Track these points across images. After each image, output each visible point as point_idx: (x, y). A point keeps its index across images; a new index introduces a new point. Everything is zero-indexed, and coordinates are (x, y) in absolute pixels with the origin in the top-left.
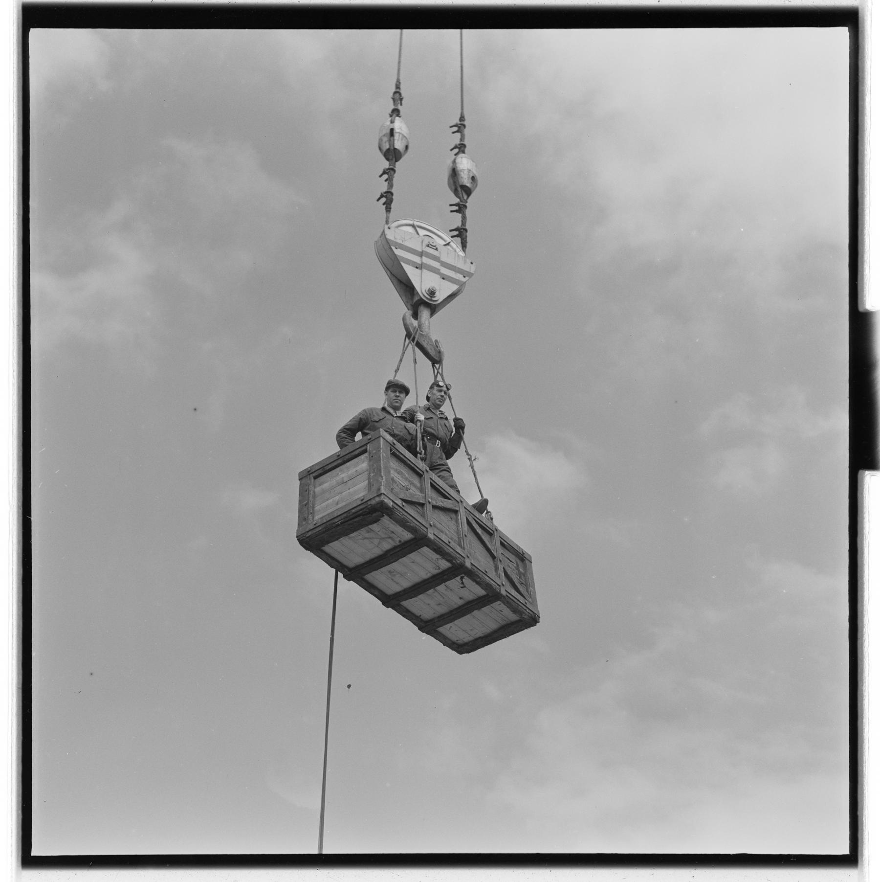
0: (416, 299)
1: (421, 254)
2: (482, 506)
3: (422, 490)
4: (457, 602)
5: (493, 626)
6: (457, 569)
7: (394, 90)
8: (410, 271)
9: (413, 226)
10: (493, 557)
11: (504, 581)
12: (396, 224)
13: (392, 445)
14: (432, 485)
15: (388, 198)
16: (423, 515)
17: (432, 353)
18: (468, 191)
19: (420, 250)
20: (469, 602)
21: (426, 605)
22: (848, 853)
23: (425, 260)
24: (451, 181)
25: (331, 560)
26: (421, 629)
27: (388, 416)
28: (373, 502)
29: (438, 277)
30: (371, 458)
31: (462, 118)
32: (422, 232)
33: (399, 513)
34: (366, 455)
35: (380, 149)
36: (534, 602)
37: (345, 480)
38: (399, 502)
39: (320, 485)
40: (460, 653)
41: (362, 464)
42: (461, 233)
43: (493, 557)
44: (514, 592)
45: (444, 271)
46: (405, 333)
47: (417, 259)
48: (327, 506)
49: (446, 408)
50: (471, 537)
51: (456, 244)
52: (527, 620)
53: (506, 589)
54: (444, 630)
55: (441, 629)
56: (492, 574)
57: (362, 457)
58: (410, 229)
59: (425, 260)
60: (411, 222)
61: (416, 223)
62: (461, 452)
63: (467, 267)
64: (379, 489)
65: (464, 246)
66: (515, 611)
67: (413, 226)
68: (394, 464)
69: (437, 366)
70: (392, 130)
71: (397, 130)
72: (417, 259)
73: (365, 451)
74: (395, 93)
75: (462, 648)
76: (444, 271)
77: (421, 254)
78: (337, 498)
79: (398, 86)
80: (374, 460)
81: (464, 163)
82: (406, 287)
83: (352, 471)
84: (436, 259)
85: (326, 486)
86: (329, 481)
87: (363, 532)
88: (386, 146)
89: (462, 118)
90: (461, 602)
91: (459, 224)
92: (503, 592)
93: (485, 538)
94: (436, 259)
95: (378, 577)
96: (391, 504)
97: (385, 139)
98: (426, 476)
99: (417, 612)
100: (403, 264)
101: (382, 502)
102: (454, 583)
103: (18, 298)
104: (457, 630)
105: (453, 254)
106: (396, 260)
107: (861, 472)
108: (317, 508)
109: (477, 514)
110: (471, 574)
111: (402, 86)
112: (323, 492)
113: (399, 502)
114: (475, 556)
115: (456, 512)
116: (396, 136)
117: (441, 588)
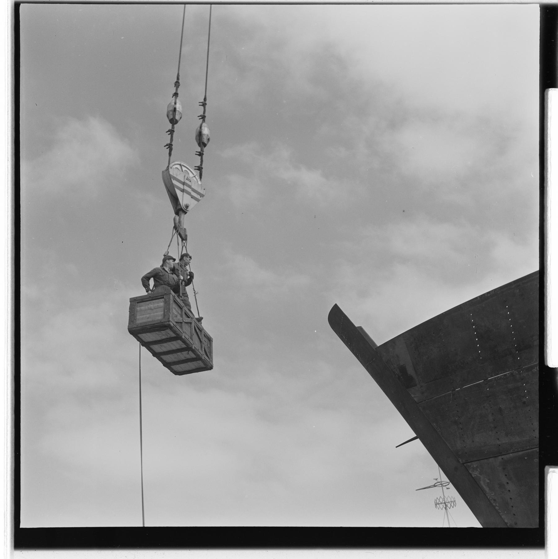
0: (179, 207)
1: (184, 184)
2: (200, 320)
3: (182, 316)
4: (183, 358)
5: (194, 367)
6: (188, 348)
7: (176, 80)
8: (178, 193)
9: (180, 165)
10: (201, 341)
11: (203, 353)
12: (173, 164)
13: (174, 297)
14: (185, 313)
15: (170, 146)
16: (181, 327)
17: (183, 236)
18: (205, 145)
19: (183, 181)
20: (188, 359)
21: (169, 358)
22: (538, 527)
23: (186, 188)
24: (198, 138)
25: (139, 339)
26: (164, 365)
27: (167, 274)
28: (166, 324)
29: (190, 197)
30: (165, 302)
31: (205, 99)
32: (184, 169)
33: (175, 328)
34: (163, 299)
35: (168, 116)
36: (212, 361)
37: (152, 308)
38: (175, 324)
39: (140, 307)
40: (176, 374)
41: (160, 303)
42: (200, 169)
43: (201, 341)
44: (206, 357)
45: (193, 194)
46: (173, 225)
47: (181, 186)
48: (143, 318)
49: (188, 267)
50: (195, 334)
51: (196, 173)
52: (209, 367)
53: (204, 357)
54: (152, 347)
55: (172, 367)
56: (200, 351)
57: (161, 300)
58: (178, 167)
59: (186, 188)
60: (179, 163)
61: (182, 164)
62: (191, 285)
63: (202, 192)
64: (169, 318)
65: (201, 177)
66: (205, 364)
67: (180, 165)
68: (174, 306)
69: (184, 241)
70: (175, 109)
71: (177, 109)
72: (181, 186)
73: (163, 298)
74: (176, 82)
75: (176, 373)
76: (193, 194)
77: (184, 184)
78: (148, 316)
79: (178, 79)
80: (167, 303)
81: (206, 131)
82: (175, 199)
83: (156, 305)
84: (190, 187)
85: (142, 308)
86: (143, 307)
87: (157, 332)
88: (171, 117)
89: (205, 99)
90: (184, 359)
91: (198, 164)
92: (203, 358)
93: (199, 333)
94: (190, 187)
95: (164, 357)
96: (172, 325)
97: (171, 113)
98: (183, 309)
99: (143, 339)
100: (176, 190)
101: (170, 325)
102: (185, 353)
103: (12, 93)
104: (177, 368)
105: (196, 183)
106: (173, 186)
107: (547, 467)
108: (138, 317)
109: (197, 323)
110: (193, 351)
111: (180, 78)
112: (141, 310)
113: (175, 324)
114: (196, 344)
115: (191, 323)
116: (177, 113)
117: (179, 354)
